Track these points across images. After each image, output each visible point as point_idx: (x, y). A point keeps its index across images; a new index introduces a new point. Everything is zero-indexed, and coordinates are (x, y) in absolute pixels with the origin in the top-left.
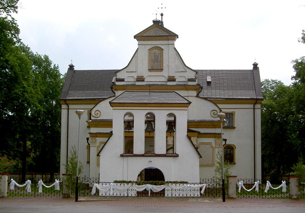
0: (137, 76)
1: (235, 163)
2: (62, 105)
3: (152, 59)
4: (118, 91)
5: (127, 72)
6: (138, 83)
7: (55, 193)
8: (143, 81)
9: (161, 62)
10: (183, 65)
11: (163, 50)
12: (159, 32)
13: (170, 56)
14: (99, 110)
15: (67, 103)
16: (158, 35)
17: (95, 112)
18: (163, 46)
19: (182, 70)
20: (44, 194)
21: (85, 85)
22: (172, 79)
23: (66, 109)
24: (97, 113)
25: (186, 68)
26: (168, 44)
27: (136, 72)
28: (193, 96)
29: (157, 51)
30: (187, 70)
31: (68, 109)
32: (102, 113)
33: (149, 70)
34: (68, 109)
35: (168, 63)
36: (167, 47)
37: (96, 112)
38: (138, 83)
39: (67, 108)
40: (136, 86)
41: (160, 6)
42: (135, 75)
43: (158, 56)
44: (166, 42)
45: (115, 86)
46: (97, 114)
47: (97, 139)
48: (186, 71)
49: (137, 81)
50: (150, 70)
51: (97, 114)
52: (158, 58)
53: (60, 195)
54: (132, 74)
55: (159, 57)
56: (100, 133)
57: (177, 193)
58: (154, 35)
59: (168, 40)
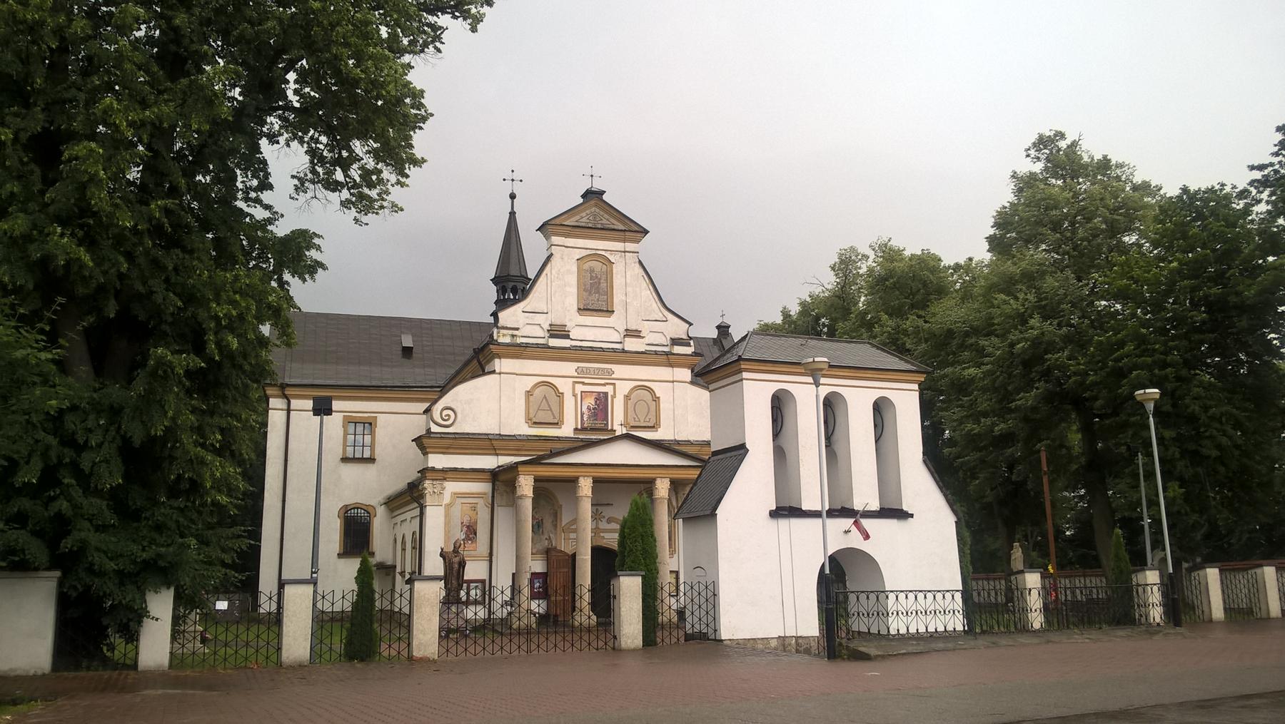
0: (551, 325)
1: (374, 553)
2: (270, 399)
3: (585, 285)
4: (502, 360)
5: (523, 312)
6: (555, 342)
7: (576, 638)
8: (567, 337)
9: (609, 293)
10: (659, 305)
11: (613, 263)
12: (602, 220)
13: (628, 281)
14: (453, 407)
15: (286, 393)
16: (599, 226)
17: (442, 410)
18: (612, 254)
19: (656, 316)
20: (450, 645)
21: (328, 349)
22: (633, 333)
23: (282, 410)
24: (449, 415)
25: (666, 313)
26: (625, 252)
27: (547, 313)
28: (686, 382)
29: (597, 266)
30: (670, 316)
31: (289, 410)
32: (459, 416)
33: (579, 309)
34: (289, 410)
35: (624, 298)
36: (621, 256)
37: (445, 412)
38: (555, 342)
39: (285, 407)
40: (549, 348)
41: (509, 176)
42: (545, 322)
43: (600, 279)
44: (619, 246)
45: (495, 344)
46: (447, 417)
47: (447, 484)
48: (667, 321)
49: (552, 336)
50: (583, 310)
51: (447, 417)
52: (600, 283)
53: (484, 649)
54: (539, 319)
55: (602, 281)
56: (455, 470)
57: (941, 603)
58: (590, 225)
59: (624, 241)
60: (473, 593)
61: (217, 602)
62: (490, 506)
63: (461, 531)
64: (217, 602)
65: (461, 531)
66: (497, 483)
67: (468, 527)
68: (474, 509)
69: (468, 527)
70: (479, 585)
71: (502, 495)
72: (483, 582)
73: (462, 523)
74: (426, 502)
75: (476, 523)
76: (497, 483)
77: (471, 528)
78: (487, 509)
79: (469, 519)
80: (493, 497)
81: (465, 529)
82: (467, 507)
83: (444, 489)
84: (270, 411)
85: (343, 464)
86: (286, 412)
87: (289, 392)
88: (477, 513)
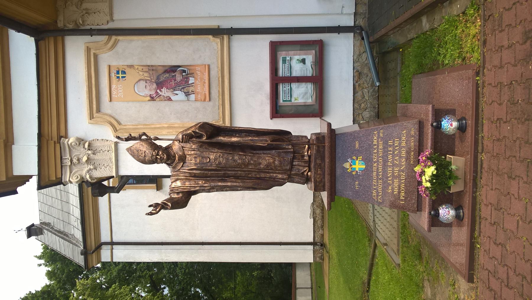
34: (112, 243)
60: (298, 70)
61: (357, 124)
62: (114, 38)
63: (170, 99)
64: (357, 124)
65: (170, 99)
66: (60, 25)
67: (160, 85)
68: (121, 73)
69: (160, 85)
70: (281, 55)
71: (88, 12)
72: (274, 47)
73: (152, 99)
74: (190, 99)
75: (151, 68)
76: (60, 25)
77: (162, 79)
78: (120, 44)
79: (142, 83)
80: (91, 32)
81: (165, 92)
82: (118, 88)
83: (80, 141)
84: (114, 261)
85: (163, 189)
86: (114, 246)
87: (92, 244)
88: (131, 66)
